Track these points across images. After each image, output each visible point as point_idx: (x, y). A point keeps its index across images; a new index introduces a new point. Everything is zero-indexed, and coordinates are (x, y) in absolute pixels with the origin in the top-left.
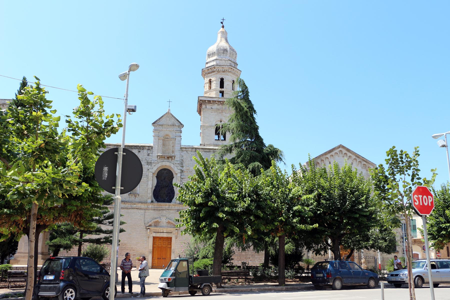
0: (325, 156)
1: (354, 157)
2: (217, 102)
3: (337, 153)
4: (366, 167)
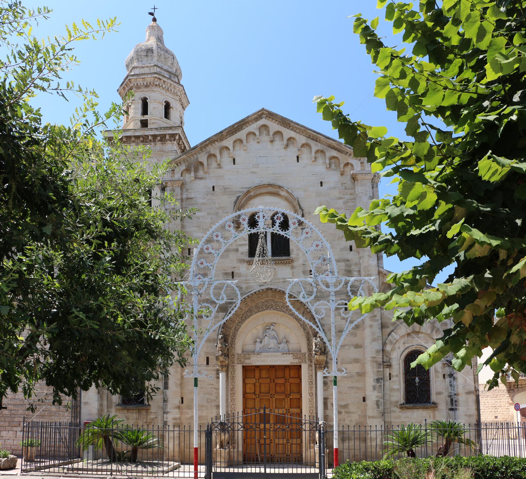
0: (218, 145)
1: (302, 139)
2: (133, 139)
3: (254, 134)
4: (338, 166)
